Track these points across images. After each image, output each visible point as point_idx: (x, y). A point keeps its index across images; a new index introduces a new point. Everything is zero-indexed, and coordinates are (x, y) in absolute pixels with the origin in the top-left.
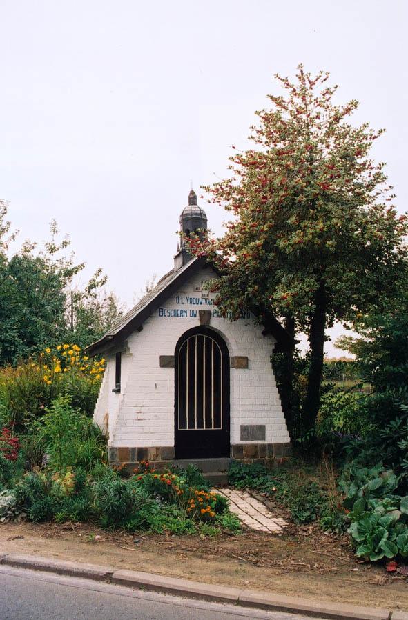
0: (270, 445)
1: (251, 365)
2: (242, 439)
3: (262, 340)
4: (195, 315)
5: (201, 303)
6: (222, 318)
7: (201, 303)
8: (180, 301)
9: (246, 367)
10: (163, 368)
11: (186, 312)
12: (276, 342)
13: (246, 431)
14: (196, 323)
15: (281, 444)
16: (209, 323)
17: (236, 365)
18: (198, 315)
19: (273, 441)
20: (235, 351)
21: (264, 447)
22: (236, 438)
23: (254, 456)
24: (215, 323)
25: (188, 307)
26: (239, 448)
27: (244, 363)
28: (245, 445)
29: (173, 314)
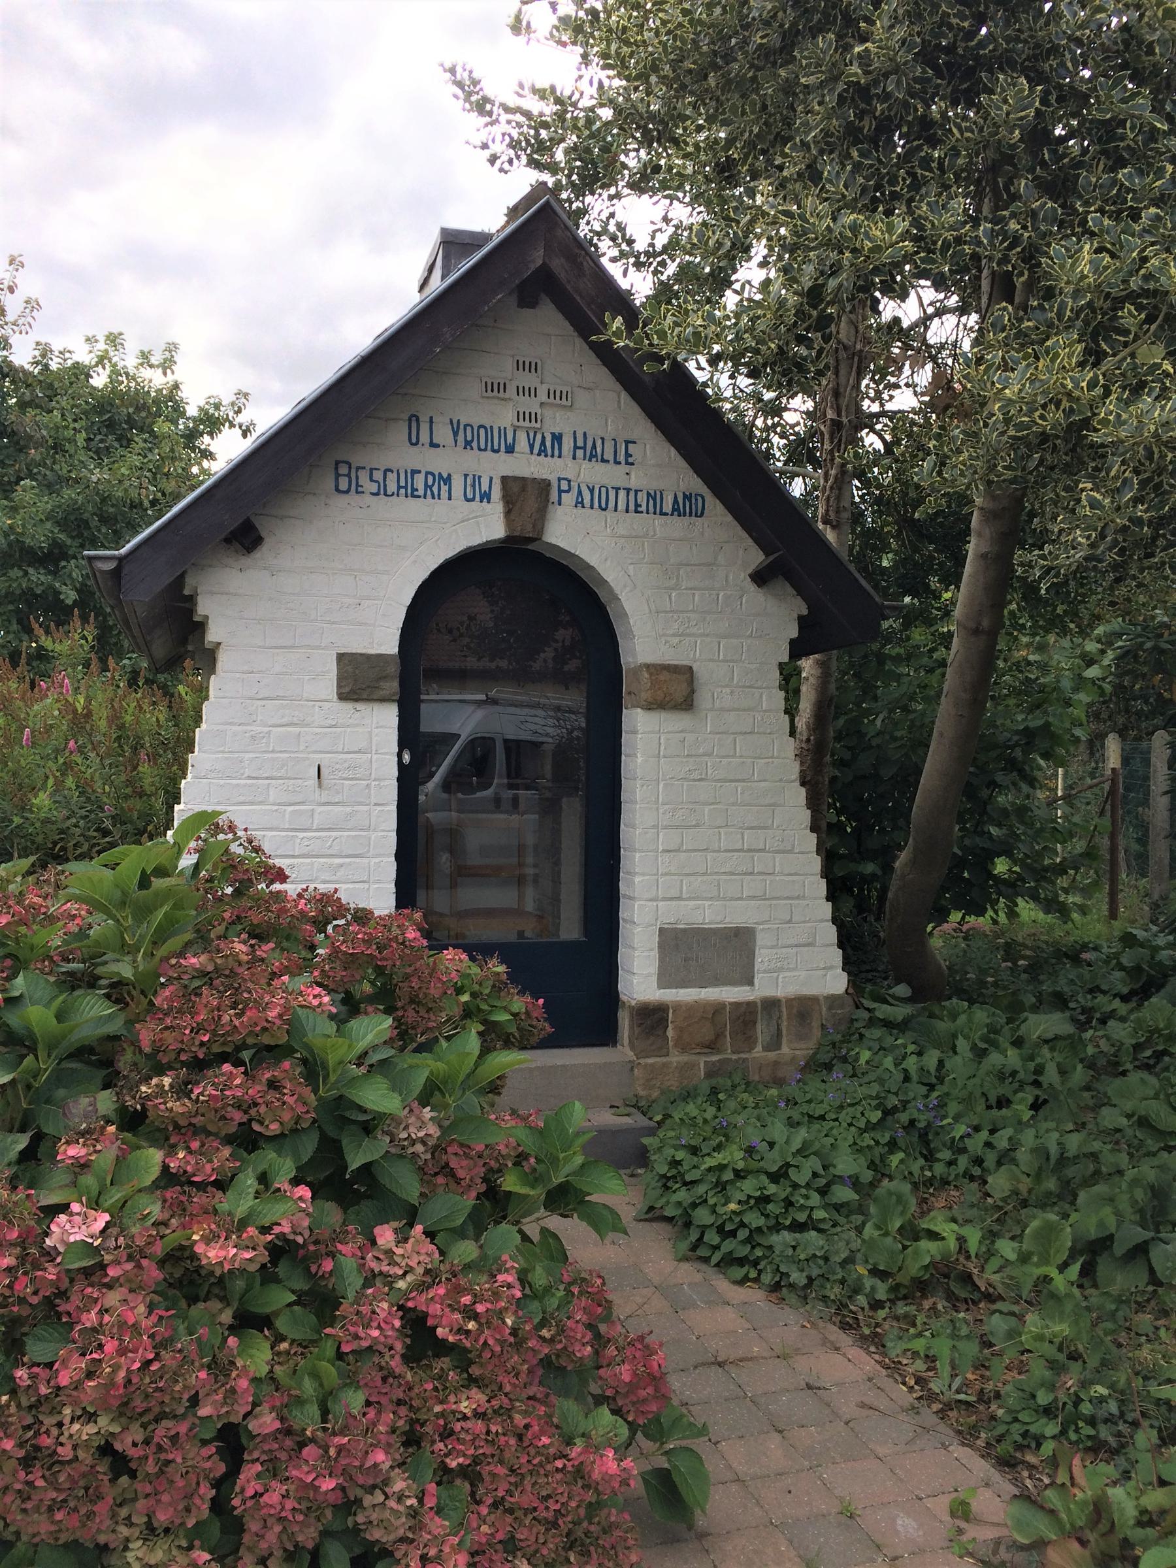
0: (771, 1004)
1: (703, 698)
2: (665, 980)
3: (755, 596)
4: (486, 497)
5: (510, 450)
6: (675, 517)
7: (510, 450)
8: (425, 437)
9: (687, 704)
10: (348, 706)
11: (448, 480)
12: (805, 612)
13: (682, 949)
14: (489, 526)
15: (814, 999)
16: (541, 531)
17: (645, 695)
18: (496, 494)
19: (780, 992)
20: (644, 641)
21: (744, 1017)
22: (640, 978)
23: (712, 1046)
24: (569, 532)
25: (450, 460)
26: (653, 1017)
27: (677, 690)
28: (678, 1006)
29: (392, 487)
